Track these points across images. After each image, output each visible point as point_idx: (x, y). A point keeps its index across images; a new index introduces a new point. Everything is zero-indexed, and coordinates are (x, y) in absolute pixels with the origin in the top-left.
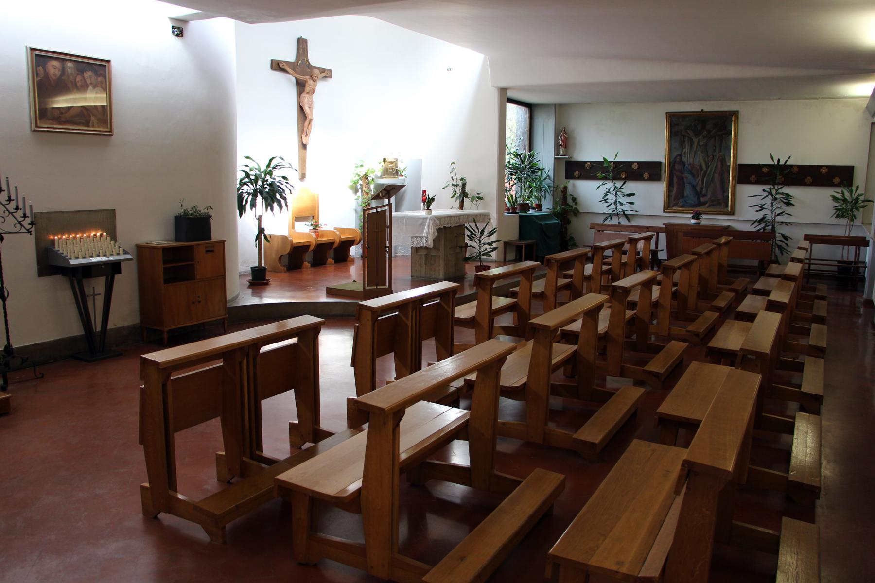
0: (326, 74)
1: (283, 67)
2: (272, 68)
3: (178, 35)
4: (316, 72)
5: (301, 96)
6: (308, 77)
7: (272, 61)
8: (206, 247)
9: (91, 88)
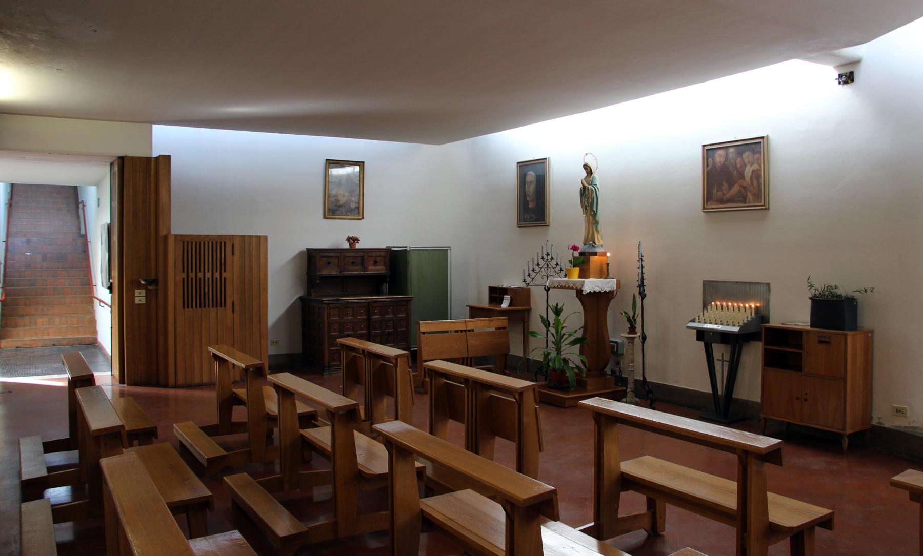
8: (819, 337)
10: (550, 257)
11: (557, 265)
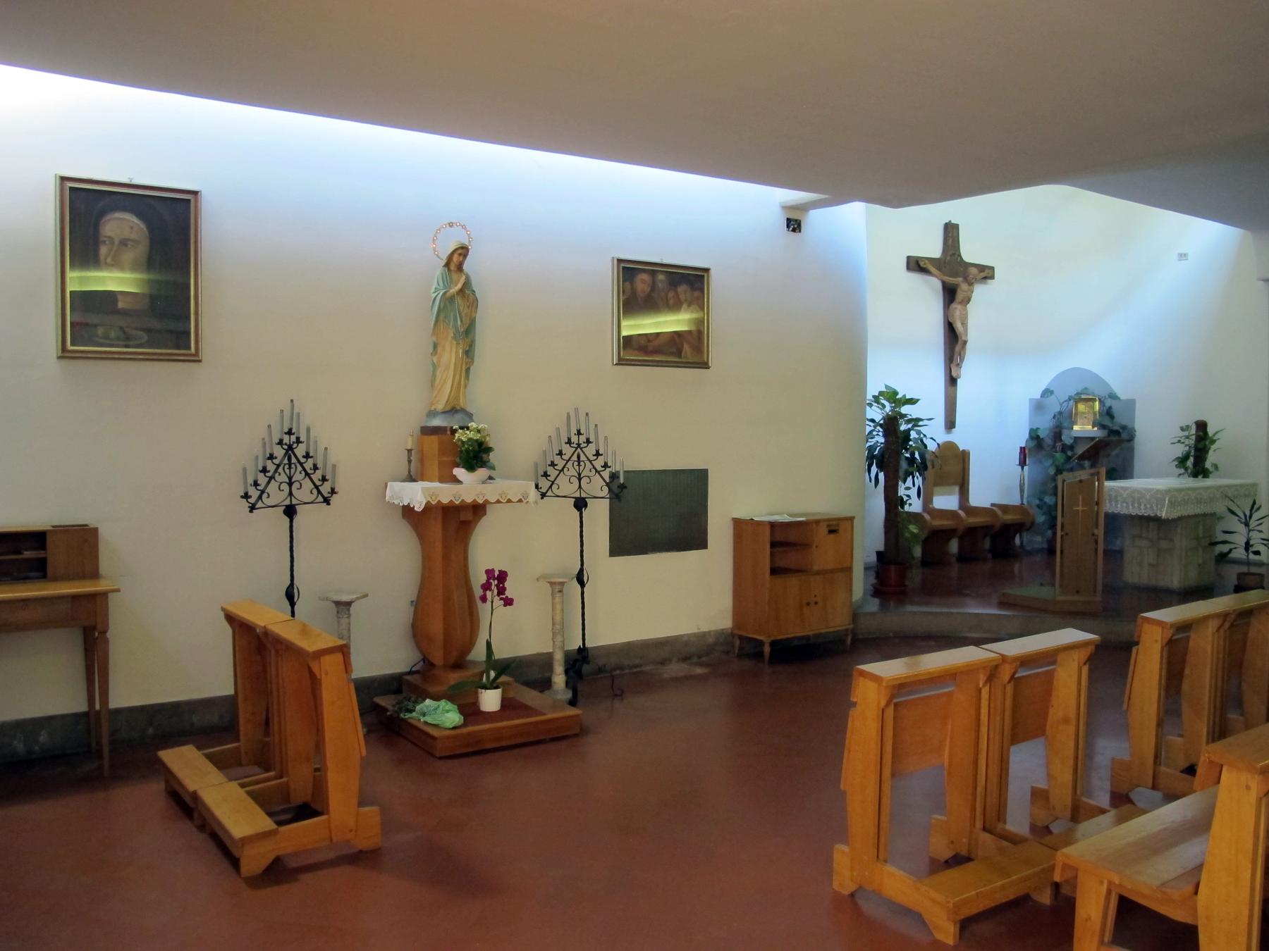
0: (986, 273)
1: (925, 266)
2: (909, 268)
3: (794, 230)
4: (974, 271)
5: (950, 307)
6: (960, 279)
7: (908, 258)
9: (685, 306)
10: (583, 439)
11: (598, 454)
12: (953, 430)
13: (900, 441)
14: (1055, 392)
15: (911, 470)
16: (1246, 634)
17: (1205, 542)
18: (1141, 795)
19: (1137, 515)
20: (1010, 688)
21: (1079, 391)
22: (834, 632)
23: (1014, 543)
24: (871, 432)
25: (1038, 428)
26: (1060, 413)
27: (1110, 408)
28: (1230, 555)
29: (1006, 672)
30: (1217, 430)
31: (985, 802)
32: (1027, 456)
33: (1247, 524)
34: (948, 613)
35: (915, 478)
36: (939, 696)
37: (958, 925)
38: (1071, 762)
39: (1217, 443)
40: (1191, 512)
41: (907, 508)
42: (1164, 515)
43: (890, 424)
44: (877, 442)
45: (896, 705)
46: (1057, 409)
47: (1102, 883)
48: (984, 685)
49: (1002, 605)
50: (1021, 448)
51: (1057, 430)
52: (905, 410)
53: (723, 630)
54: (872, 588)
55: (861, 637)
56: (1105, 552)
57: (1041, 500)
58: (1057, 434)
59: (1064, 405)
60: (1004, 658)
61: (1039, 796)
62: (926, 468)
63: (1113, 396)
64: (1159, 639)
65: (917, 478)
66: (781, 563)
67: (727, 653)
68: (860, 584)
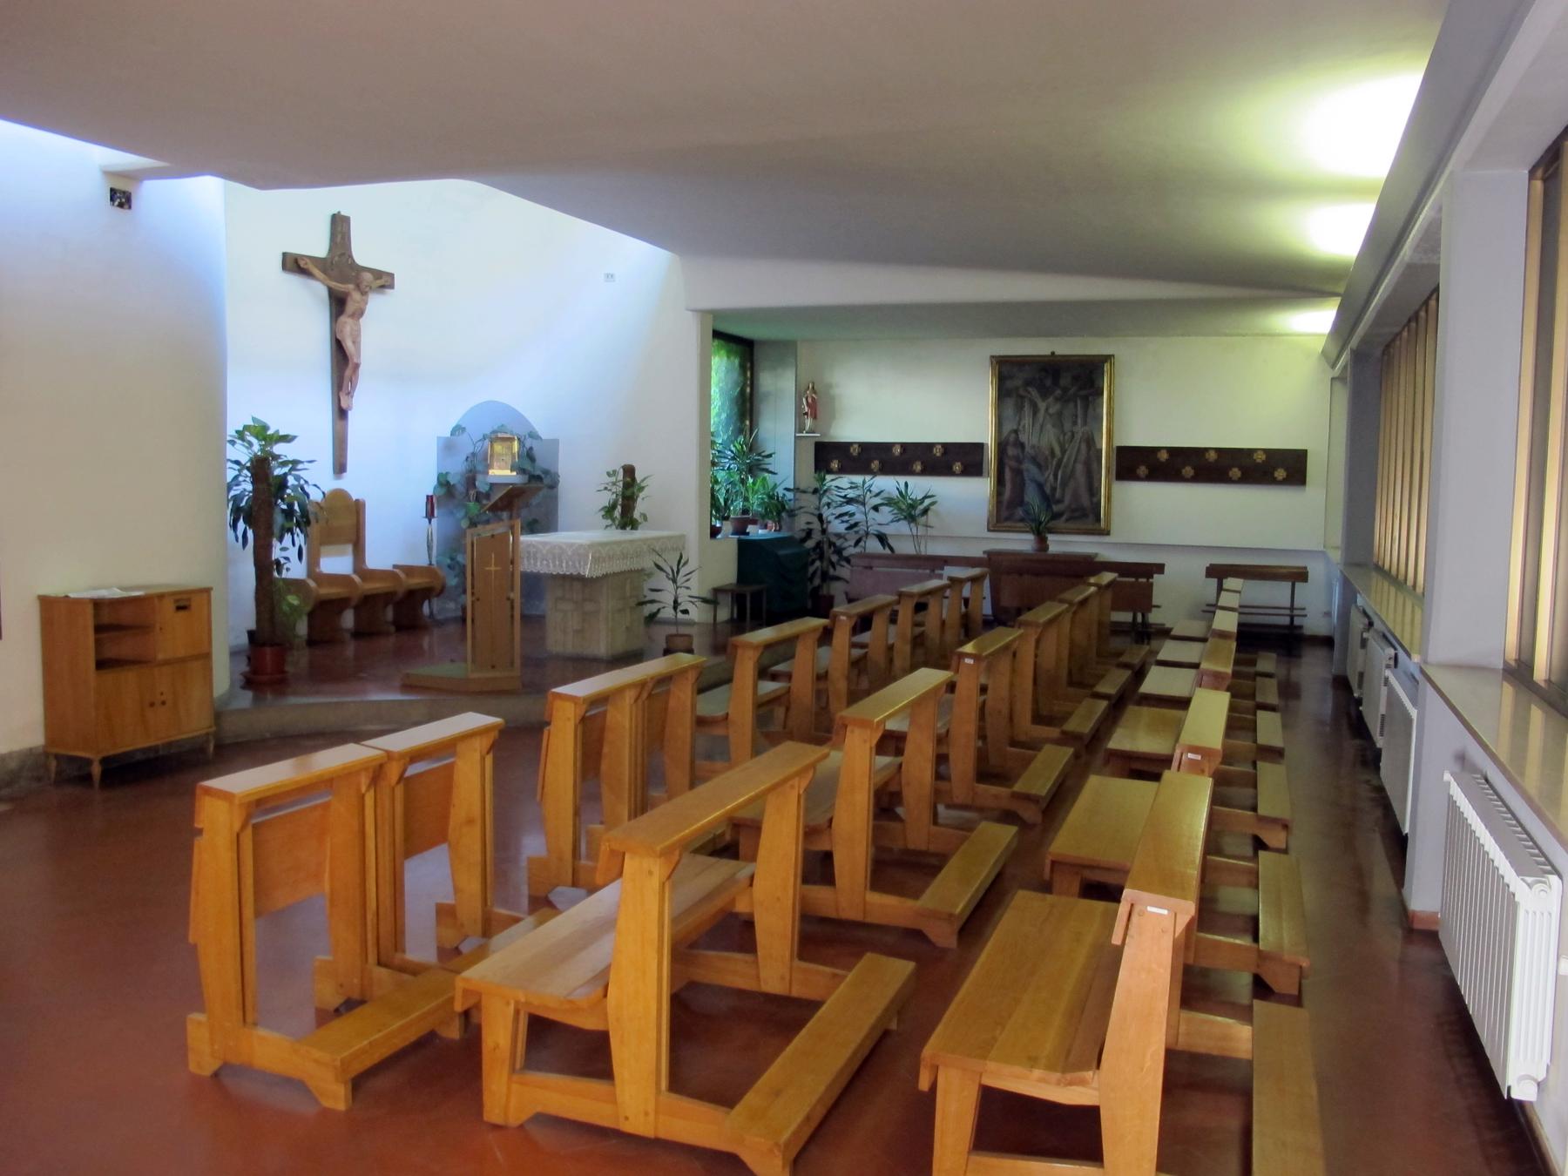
0: (384, 281)
1: (305, 267)
2: (285, 267)
3: (121, 205)
4: (368, 276)
6: (351, 286)
7: (285, 255)
12: (344, 474)
13: (273, 489)
14: (467, 430)
15: (287, 525)
16: (667, 703)
17: (633, 602)
18: (560, 894)
19: (558, 574)
20: (399, 791)
21: (495, 428)
22: (189, 738)
23: (422, 611)
24: (236, 478)
25: (447, 473)
26: (474, 454)
27: (531, 449)
28: (659, 616)
29: (393, 772)
30: (646, 476)
31: (378, 932)
32: (435, 506)
33: (674, 581)
34: (336, 703)
35: (295, 536)
36: (315, 808)
37: (350, 1086)
38: (479, 869)
39: (646, 489)
40: (617, 569)
41: (285, 574)
42: (587, 573)
43: (260, 468)
44: (245, 490)
45: (256, 827)
46: (471, 450)
47: (508, 1004)
48: (368, 790)
49: (408, 687)
50: (428, 497)
51: (470, 475)
52: (278, 449)
53: (31, 749)
54: (241, 677)
55: (228, 741)
56: (523, 617)
57: (452, 559)
58: (470, 480)
59: (477, 445)
60: (389, 755)
61: (445, 913)
62: (308, 523)
63: (533, 435)
64: (572, 716)
65: (298, 535)
66: (111, 652)
67: (39, 779)
68: (223, 675)
